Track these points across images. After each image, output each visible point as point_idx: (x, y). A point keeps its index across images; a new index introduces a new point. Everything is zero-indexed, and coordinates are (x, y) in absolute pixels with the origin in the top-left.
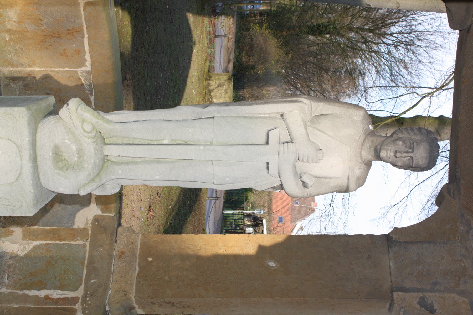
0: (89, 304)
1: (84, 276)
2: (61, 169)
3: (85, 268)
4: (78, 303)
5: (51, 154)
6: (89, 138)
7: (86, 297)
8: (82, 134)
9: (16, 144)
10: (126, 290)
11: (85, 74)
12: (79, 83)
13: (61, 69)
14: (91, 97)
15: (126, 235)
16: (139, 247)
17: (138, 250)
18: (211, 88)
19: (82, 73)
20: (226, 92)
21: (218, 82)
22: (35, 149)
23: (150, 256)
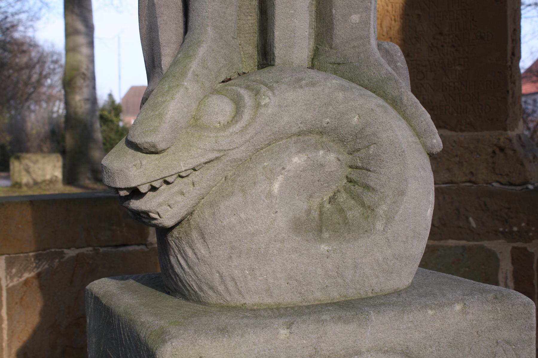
0: (528, 224)
1: (462, 243)
2: (369, 210)
3: (442, 243)
4: (525, 249)
5: (324, 247)
6: (258, 106)
7: (511, 232)
8: (246, 127)
10: (490, 150)
11: (14, 271)
12: (36, 283)
13: (5, 325)
14: (67, 256)
18: (31, 181)
19: (12, 278)
20: (36, 162)
21: (24, 173)
22: (308, 307)
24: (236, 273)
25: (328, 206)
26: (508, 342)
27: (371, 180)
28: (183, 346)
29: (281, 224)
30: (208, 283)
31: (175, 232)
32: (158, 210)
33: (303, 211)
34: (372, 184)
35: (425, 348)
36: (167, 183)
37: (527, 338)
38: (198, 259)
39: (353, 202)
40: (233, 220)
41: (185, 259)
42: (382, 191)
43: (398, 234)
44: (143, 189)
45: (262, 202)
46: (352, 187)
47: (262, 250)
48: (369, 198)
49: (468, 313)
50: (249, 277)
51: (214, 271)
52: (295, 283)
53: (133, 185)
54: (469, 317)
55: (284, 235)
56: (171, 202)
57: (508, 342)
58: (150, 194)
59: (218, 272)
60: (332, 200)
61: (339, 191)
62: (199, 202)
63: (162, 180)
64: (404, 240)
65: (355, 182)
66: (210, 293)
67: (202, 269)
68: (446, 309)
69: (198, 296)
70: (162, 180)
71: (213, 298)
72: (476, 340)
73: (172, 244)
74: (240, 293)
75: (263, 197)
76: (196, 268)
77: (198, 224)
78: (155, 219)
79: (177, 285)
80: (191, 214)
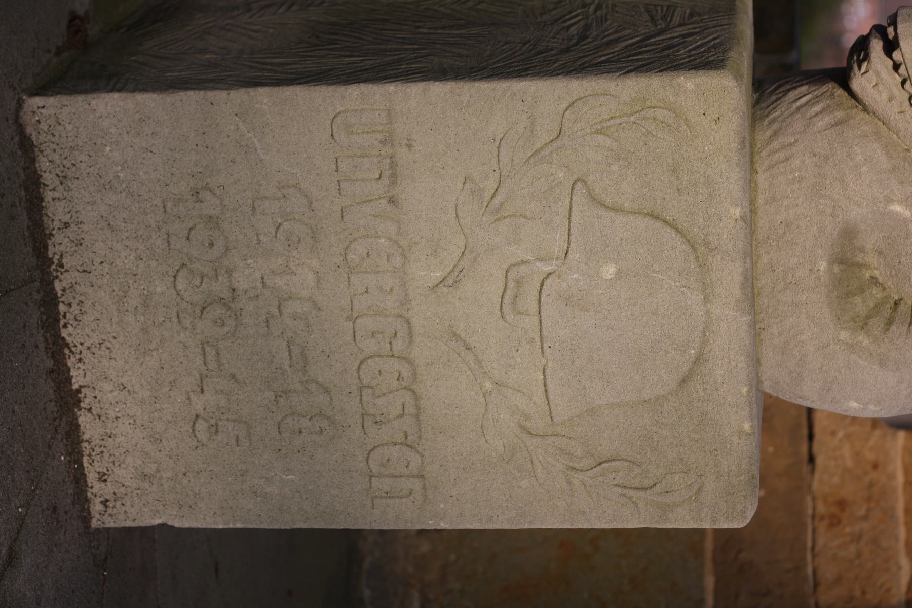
2: (863, 324)
3: (709, 565)
5: (823, 265)
9: (683, 235)
15: (848, 436)
16: (900, 479)
24: (797, 162)
25: (867, 275)
26: (700, 490)
27: (898, 328)
28: (732, 99)
29: (854, 213)
30: (780, 129)
31: (840, 92)
32: (871, 72)
33: (864, 243)
34: (894, 328)
35: (703, 383)
36: (903, 83)
37: (703, 515)
38: (811, 118)
39: (872, 305)
40: (860, 158)
41: (807, 103)
42: (886, 340)
43: (833, 359)
44: (896, 55)
45: (880, 191)
46: (889, 305)
47: (823, 192)
48: (876, 324)
49: (740, 438)
50: (791, 177)
51: (797, 136)
52: (781, 231)
53: (902, 43)
54: (735, 439)
55: (841, 217)
56: (881, 87)
57: (700, 490)
58: (890, 63)
59: (796, 141)
60: (874, 280)
61: (884, 289)
62: (879, 119)
63: (907, 75)
64: (824, 369)
65: (895, 309)
66: (769, 133)
67: (798, 124)
68: (748, 409)
69: (762, 119)
70: (907, 75)
71: (762, 136)
72: (707, 447)
73: (824, 88)
74: (771, 167)
75: (885, 192)
76: (798, 116)
77: (852, 118)
78: (860, 68)
79: (771, 93)
80: (865, 109)
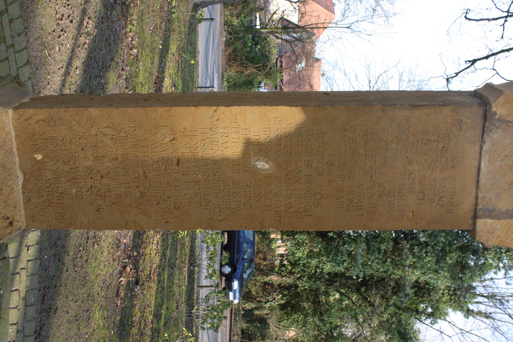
16: (13, 134)
17: (14, 140)
23: (37, 151)
